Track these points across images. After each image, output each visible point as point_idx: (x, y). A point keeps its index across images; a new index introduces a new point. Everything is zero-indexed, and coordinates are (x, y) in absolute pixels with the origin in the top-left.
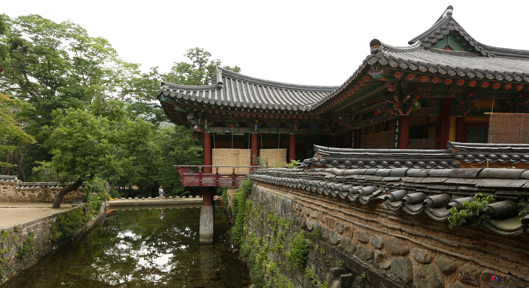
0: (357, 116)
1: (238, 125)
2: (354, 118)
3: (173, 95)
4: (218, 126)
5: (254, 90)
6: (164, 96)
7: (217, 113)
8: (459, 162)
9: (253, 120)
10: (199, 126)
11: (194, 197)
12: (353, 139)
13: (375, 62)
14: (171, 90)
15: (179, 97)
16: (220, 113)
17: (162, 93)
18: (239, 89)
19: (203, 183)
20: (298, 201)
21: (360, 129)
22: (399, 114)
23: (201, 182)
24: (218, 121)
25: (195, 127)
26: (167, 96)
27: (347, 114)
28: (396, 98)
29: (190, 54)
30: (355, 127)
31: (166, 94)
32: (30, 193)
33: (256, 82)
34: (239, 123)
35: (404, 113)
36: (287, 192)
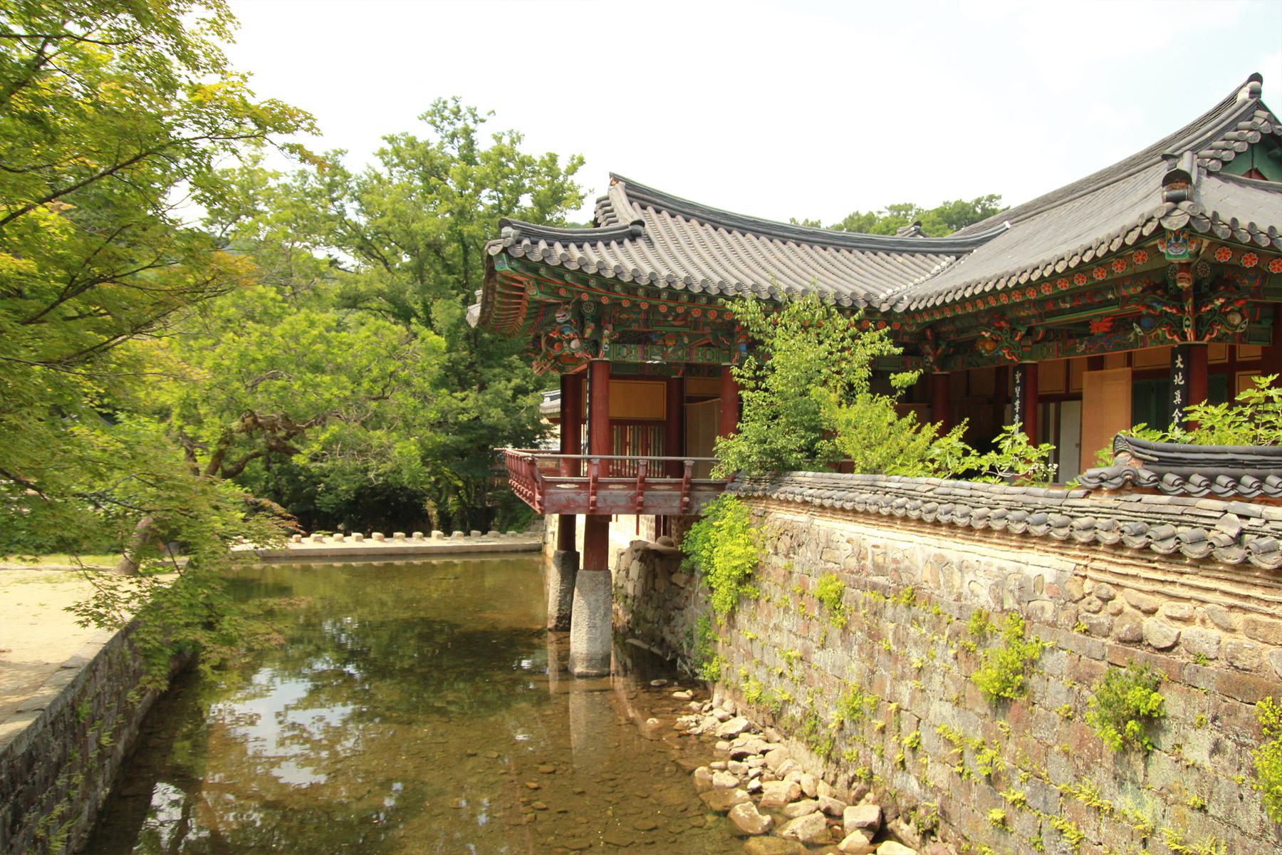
0: (1030, 332)
1: (686, 340)
2: (1023, 337)
3: (536, 257)
4: (631, 342)
6: (510, 258)
7: (626, 304)
8: (311, 293)
10: (582, 339)
11: (389, 534)
12: (1018, 390)
13: (1183, 224)
14: (526, 242)
15: (554, 262)
16: (654, 309)
20: (1090, 573)
22: (1186, 338)
24: (635, 327)
25: (574, 344)
26: (518, 259)
27: (1003, 323)
28: (1188, 306)
29: (436, 114)
30: (1022, 358)
31: (519, 252)
33: (718, 219)
35: (1196, 339)
36: (1020, 548)
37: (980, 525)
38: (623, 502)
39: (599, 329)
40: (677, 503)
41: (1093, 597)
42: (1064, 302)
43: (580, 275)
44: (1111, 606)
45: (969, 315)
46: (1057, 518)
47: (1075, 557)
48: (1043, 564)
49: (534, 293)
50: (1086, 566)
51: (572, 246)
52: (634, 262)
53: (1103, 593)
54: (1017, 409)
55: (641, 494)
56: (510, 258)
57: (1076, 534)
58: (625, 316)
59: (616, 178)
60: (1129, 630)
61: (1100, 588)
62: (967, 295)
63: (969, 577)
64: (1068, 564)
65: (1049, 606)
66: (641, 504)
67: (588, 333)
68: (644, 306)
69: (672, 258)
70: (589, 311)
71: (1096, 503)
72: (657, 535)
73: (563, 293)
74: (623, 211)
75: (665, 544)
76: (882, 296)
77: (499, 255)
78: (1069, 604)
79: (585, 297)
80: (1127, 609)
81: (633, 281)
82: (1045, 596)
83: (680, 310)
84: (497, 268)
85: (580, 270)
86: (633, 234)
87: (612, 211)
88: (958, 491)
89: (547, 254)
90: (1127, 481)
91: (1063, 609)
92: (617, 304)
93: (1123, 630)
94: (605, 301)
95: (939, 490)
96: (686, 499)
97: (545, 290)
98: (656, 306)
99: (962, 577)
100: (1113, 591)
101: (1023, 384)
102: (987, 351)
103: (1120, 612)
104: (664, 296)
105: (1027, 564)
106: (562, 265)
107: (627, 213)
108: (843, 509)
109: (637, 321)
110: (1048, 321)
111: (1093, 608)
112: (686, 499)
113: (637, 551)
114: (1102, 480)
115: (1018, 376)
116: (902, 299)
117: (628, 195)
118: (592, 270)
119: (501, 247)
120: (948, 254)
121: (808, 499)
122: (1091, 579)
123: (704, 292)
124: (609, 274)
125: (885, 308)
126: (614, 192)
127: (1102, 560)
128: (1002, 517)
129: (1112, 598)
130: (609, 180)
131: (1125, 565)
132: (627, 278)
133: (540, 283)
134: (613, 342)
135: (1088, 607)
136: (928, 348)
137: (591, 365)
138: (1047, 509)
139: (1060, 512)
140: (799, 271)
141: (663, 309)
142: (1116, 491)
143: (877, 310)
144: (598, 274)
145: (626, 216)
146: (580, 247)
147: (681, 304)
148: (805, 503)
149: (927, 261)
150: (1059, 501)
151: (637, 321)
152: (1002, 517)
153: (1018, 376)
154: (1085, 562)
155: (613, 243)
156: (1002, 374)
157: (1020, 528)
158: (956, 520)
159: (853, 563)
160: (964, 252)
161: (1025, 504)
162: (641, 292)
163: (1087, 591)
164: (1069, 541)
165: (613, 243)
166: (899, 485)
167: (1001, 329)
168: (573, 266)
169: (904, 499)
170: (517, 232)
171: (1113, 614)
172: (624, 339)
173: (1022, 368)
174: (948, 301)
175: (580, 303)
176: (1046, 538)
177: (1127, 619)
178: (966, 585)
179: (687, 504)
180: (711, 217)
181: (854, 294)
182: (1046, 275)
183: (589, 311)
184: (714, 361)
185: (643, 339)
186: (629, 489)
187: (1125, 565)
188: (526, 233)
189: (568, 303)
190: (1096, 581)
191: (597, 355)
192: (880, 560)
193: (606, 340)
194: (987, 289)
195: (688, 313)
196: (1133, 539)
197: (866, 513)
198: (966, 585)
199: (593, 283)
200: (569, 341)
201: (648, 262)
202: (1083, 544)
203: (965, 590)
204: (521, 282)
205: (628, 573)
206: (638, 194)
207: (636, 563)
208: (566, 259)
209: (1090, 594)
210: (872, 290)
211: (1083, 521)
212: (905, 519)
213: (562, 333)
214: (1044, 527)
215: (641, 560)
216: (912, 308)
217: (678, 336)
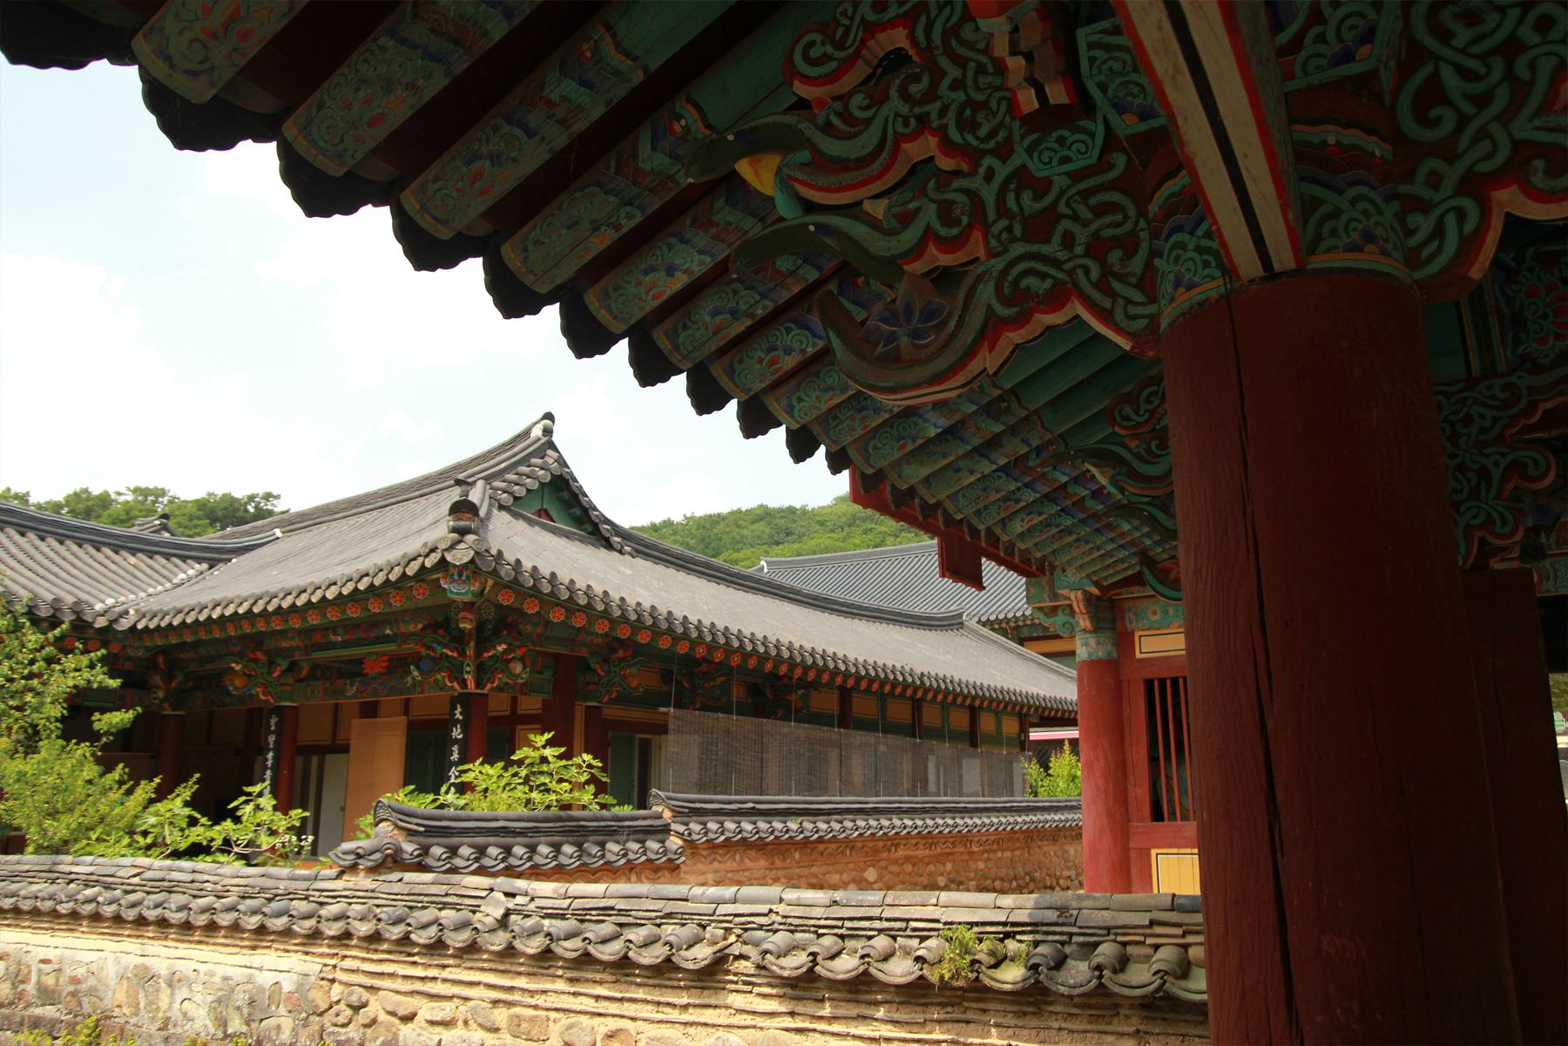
0: (293, 667)
12: (272, 739)
27: (259, 655)
30: (281, 699)
36: (254, 948)
37: (202, 920)
42: (336, 634)
45: (216, 641)
46: (301, 906)
54: (269, 763)
57: (517, 944)
71: (350, 885)
76: (99, 607)
88: (175, 875)
95: (149, 874)
102: (236, 688)
110: (316, 655)
114: (359, 856)
115: (273, 721)
116: (127, 613)
120: (199, 560)
125: (101, 623)
128: (232, 908)
138: (290, 895)
139: (306, 898)
142: (374, 870)
149: (169, 566)
150: (305, 885)
152: (232, 908)
153: (273, 721)
156: (255, 717)
158: (168, 914)
160: (221, 561)
161: (263, 890)
164: (315, 936)
167: (256, 661)
173: (279, 711)
176: (287, 933)
202: (332, 938)
211: (334, 909)
212: (96, 918)
214: (285, 919)
216: (140, 626)
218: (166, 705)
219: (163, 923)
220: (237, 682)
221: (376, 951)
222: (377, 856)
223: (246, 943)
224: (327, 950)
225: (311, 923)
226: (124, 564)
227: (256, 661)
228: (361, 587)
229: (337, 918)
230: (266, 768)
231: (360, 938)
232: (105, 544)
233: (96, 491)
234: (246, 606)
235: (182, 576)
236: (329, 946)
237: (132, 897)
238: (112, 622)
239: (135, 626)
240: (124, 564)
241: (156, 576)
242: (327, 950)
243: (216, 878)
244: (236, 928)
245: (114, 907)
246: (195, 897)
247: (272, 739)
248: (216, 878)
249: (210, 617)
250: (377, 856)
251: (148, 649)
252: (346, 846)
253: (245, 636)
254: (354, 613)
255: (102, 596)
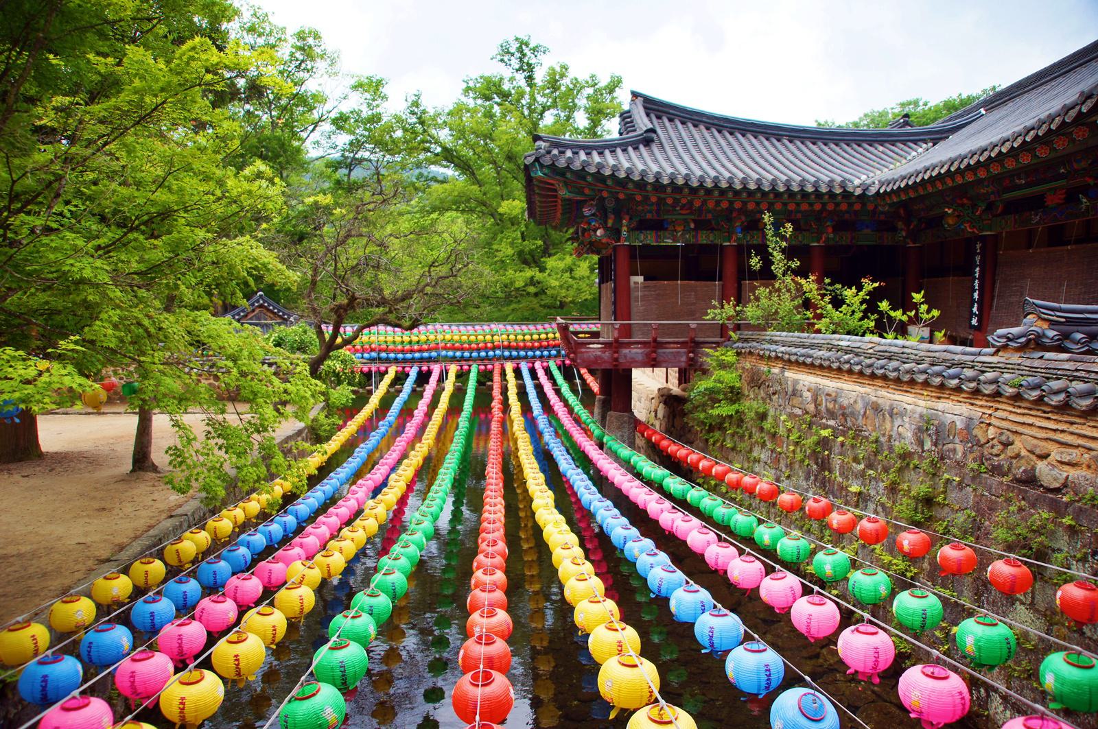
0: (990, 206)
1: (692, 226)
2: (983, 211)
3: (562, 163)
4: (646, 229)
5: (683, 134)
6: (542, 166)
7: (639, 198)
9: (728, 215)
10: (606, 228)
12: (978, 258)
14: (555, 152)
16: (661, 201)
17: (537, 160)
18: (689, 144)
19: (621, 360)
20: (993, 421)
21: (996, 237)
23: (616, 360)
24: (649, 216)
25: (599, 233)
26: (548, 166)
27: (965, 201)
30: (983, 230)
31: (547, 161)
32: (212, 381)
34: (694, 221)
36: (939, 398)
37: (906, 378)
38: (640, 358)
39: (619, 219)
40: (684, 359)
41: (995, 442)
42: (1020, 179)
43: (598, 176)
44: (1011, 451)
45: (929, 195)
46: (969, 373)
47: (981, 406)
48: (954, 411)
49: (564, 193)
50: (990, 415)
51: (595, 154)
52: (785, 175)
53: (1003, 438)
54: (977, 275)
55: (655, 352)
56: (542, 166)
57: (981, 387)
58: (640, 208)
59: (635, 95)
60: (1024, 471)
61: (1001, 434)
62: (926, 178)
63: (898, 422)
64: (976, 413)
65: (960, 448)
66: (654, 359)
67: (610, 223)
68: (654, 199)
69: (680, 160)
70: (610, 205)
71: (1003, 360)
72: (680, 384)
73: (587, 191)
74: (639, 121)
75: (684, 390)
76: (857, 182)
77: (533, 164)
78: (975, 447)
79: (605, 194)
80: (1024, 453)
81: (642, 179)
82: (957, 440)
83: (684, 201)
84: (532, 175)
85: (598, 172)
86: (648, 140)
87: (632, 122)
88: (893, 349)
89: (570, 161)
90: (1030, 340)
91: (971, 452)
92: (631, 198)
93: (1020, 470)
94: (621, 196)
95: (878, 348)
96: (691, 355)
97: (572, 190)
98: (664, 199)
99: (892, 422)
100: (1012, 437)
101: (983, 254)
102: (949, 225)
103: (1018, 456)
104: (669, 190)
105: (943, 412)
106: (583, 169)
107: (643, 122)
108: (804, 364)
109: (651, 212)
110: (1005, 196)
111: (995, 451)
112: (691, 355)
113: (662, 396)
114: (1009, 340)
115: (978, 246)
116: (874, 183)
117: (645, 108)
118: (607, 172)
119: (534, 157)
120: (925, 142)
121: (780, 355)
122: (995, 426)
123: (716, 186)
124: (622, 175)
125: (858, 192)
126: (634, 106)
127: (1004, 410)
128: (925, 372)
129: (1012, 443)
130: (630, 97)
131: (1024, 414)
132: (636, 177)
133: (567, 184)
134: (630, 230)
135: (990, 451)
136: (900, 225)
137: (615, 248)
138: (962, 365)
139: (973, 367)
140: (787, 163)
141: (670, 201)
142: (1022, 348)
143: (852, 194)
144: (613, 175)
145: (642, 126)
146: (600, 154)
147: (684, 197)
148: (777, 358)
149: (906, 148)
150: (972, 358)
151: (651, 212)
152: (925, 372)
153: (978, 246)
154: (989, 412)
155: (630, 149)
156: (970, 242)
157: (937, 380)
158: (888, 373)
159: (811, 408)
160: (941, 139)
161: (944, 360)
162: (649, 188)
163: (991, 437)
164: (976, 393)
165: (630, 149)
166: (848, 343)
167: (963, 205)
168: (593, 170)
169: (851, 356)
170: (547, 144)
171: (1012, 458)
172: (643, 225)
173: (983, 239)
174: (910, 183)
175: (602, 199)
176: (958, 390)
177: (1023, 461)
178: (895, 428)
179: (691, 359)
180: (716, 122)
181: (832, 181)
182: (993, 155)
183: (610, 205)
184: (805, 242)
185: (658, 226)
186: (644, 347)
187: (1024, 414)
188: (555, 144)
189: (593, 200)
190: (999, 428)
191: (619, 240)
192: (831, 406)
193: (625, 228)
194: (943, 171)
195: (691, 203)
196: (1030, 392)
197: (821, 367)
198: (895, 428)
199: (609, 183)
200: (595, 231)
201: (713, 168)
202: (988, 396)
203: (894, 434)
204: (552, 185)
205: (656, 413)
206: (654, 107)
207: (661, 405)
208: (585, 164)
209: (993, 439)
210: (848, 176)
211: (990, 376)
212: (850, 372)
213: (589, 224)
214: (956, 381)
215: (665, 403)
216: (881, 191)
217: (686, 222)
218: (908, 240)
219: (884, 378)
220: (951, 222)
221: (1020, 407)
222: (1023, 340)
223: (933, 394)
224: (985, 404)
225: (973, 385)
226: (875, 152)
227: (963, 205)
228: (1028, 139)
229: (992, 382)
230: (975, 278)
231: (1008, 398)
232: (863, 141)
233: (964, 96)
234: (946, 168)
235: (914, 153)
236: (987, 401)
237: (868, 361)
238: (864, 190)
239: (878, 191)
240: (875, 152)
241: (895, 156)
242: (985, 404)
243: (916, 352)
244: (926, 384)
245: (859, 367)
246: (904, 363)
247: (978, 258)
248: (916, 352)
249: (915, 182)
250: (1023, 340)
251: (891, 205)
252: (1000, 332)
253: (953, 189)
254: (1025, 160)
255: (858, 174)
